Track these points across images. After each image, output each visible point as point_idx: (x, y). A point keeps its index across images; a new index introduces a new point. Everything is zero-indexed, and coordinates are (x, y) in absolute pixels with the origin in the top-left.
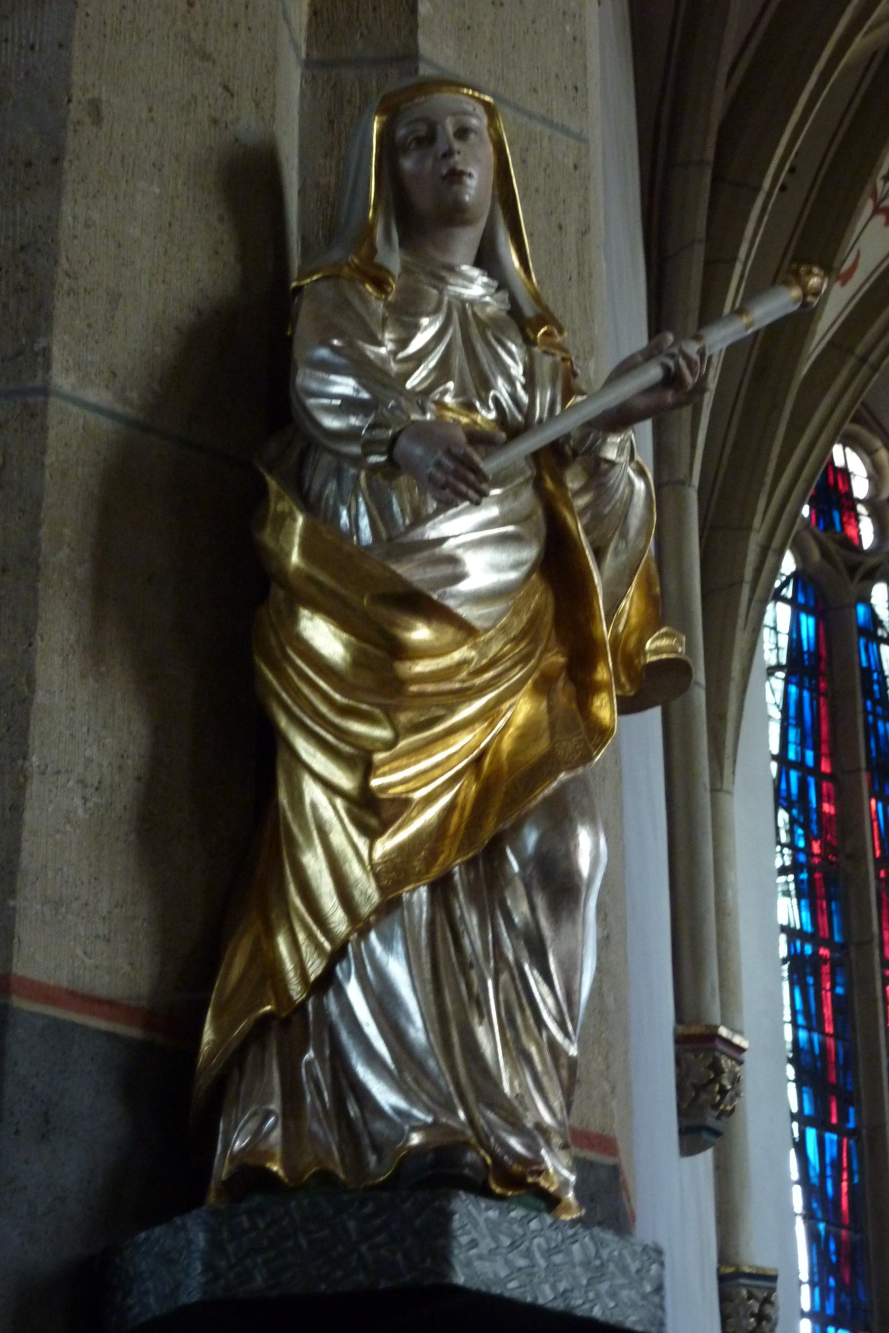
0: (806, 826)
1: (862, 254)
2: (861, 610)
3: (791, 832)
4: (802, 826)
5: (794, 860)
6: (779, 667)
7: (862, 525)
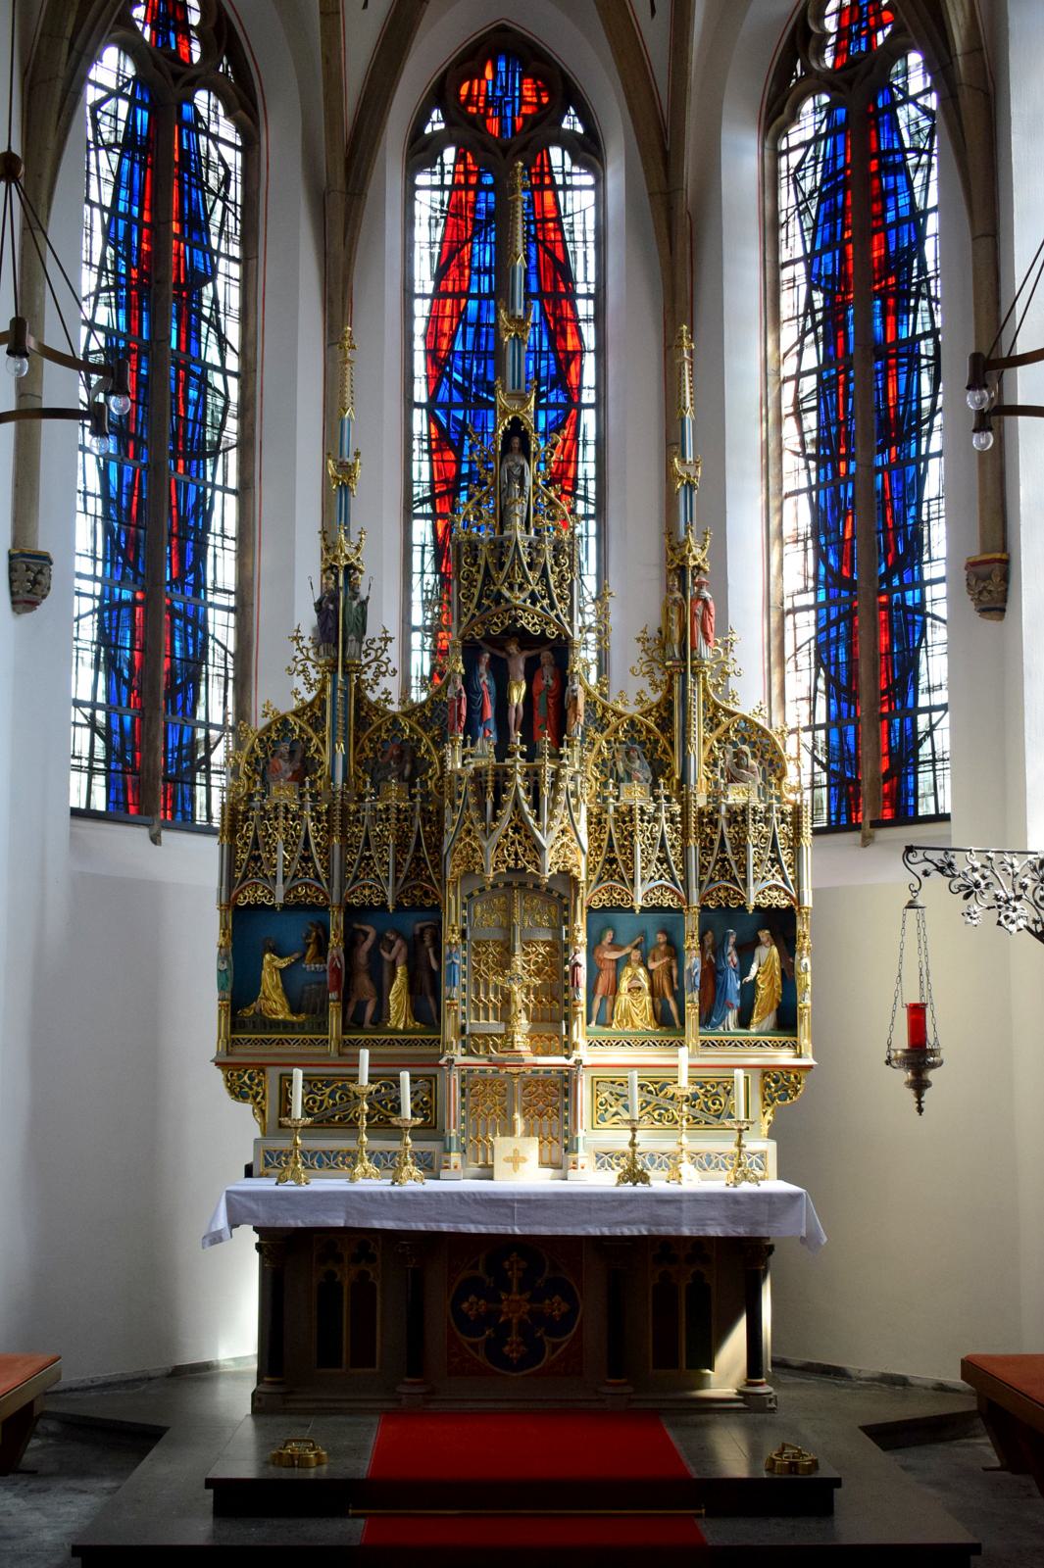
2: (187, 109)
3: (115, 263)
4: (124, 259)
6: (116, 144)
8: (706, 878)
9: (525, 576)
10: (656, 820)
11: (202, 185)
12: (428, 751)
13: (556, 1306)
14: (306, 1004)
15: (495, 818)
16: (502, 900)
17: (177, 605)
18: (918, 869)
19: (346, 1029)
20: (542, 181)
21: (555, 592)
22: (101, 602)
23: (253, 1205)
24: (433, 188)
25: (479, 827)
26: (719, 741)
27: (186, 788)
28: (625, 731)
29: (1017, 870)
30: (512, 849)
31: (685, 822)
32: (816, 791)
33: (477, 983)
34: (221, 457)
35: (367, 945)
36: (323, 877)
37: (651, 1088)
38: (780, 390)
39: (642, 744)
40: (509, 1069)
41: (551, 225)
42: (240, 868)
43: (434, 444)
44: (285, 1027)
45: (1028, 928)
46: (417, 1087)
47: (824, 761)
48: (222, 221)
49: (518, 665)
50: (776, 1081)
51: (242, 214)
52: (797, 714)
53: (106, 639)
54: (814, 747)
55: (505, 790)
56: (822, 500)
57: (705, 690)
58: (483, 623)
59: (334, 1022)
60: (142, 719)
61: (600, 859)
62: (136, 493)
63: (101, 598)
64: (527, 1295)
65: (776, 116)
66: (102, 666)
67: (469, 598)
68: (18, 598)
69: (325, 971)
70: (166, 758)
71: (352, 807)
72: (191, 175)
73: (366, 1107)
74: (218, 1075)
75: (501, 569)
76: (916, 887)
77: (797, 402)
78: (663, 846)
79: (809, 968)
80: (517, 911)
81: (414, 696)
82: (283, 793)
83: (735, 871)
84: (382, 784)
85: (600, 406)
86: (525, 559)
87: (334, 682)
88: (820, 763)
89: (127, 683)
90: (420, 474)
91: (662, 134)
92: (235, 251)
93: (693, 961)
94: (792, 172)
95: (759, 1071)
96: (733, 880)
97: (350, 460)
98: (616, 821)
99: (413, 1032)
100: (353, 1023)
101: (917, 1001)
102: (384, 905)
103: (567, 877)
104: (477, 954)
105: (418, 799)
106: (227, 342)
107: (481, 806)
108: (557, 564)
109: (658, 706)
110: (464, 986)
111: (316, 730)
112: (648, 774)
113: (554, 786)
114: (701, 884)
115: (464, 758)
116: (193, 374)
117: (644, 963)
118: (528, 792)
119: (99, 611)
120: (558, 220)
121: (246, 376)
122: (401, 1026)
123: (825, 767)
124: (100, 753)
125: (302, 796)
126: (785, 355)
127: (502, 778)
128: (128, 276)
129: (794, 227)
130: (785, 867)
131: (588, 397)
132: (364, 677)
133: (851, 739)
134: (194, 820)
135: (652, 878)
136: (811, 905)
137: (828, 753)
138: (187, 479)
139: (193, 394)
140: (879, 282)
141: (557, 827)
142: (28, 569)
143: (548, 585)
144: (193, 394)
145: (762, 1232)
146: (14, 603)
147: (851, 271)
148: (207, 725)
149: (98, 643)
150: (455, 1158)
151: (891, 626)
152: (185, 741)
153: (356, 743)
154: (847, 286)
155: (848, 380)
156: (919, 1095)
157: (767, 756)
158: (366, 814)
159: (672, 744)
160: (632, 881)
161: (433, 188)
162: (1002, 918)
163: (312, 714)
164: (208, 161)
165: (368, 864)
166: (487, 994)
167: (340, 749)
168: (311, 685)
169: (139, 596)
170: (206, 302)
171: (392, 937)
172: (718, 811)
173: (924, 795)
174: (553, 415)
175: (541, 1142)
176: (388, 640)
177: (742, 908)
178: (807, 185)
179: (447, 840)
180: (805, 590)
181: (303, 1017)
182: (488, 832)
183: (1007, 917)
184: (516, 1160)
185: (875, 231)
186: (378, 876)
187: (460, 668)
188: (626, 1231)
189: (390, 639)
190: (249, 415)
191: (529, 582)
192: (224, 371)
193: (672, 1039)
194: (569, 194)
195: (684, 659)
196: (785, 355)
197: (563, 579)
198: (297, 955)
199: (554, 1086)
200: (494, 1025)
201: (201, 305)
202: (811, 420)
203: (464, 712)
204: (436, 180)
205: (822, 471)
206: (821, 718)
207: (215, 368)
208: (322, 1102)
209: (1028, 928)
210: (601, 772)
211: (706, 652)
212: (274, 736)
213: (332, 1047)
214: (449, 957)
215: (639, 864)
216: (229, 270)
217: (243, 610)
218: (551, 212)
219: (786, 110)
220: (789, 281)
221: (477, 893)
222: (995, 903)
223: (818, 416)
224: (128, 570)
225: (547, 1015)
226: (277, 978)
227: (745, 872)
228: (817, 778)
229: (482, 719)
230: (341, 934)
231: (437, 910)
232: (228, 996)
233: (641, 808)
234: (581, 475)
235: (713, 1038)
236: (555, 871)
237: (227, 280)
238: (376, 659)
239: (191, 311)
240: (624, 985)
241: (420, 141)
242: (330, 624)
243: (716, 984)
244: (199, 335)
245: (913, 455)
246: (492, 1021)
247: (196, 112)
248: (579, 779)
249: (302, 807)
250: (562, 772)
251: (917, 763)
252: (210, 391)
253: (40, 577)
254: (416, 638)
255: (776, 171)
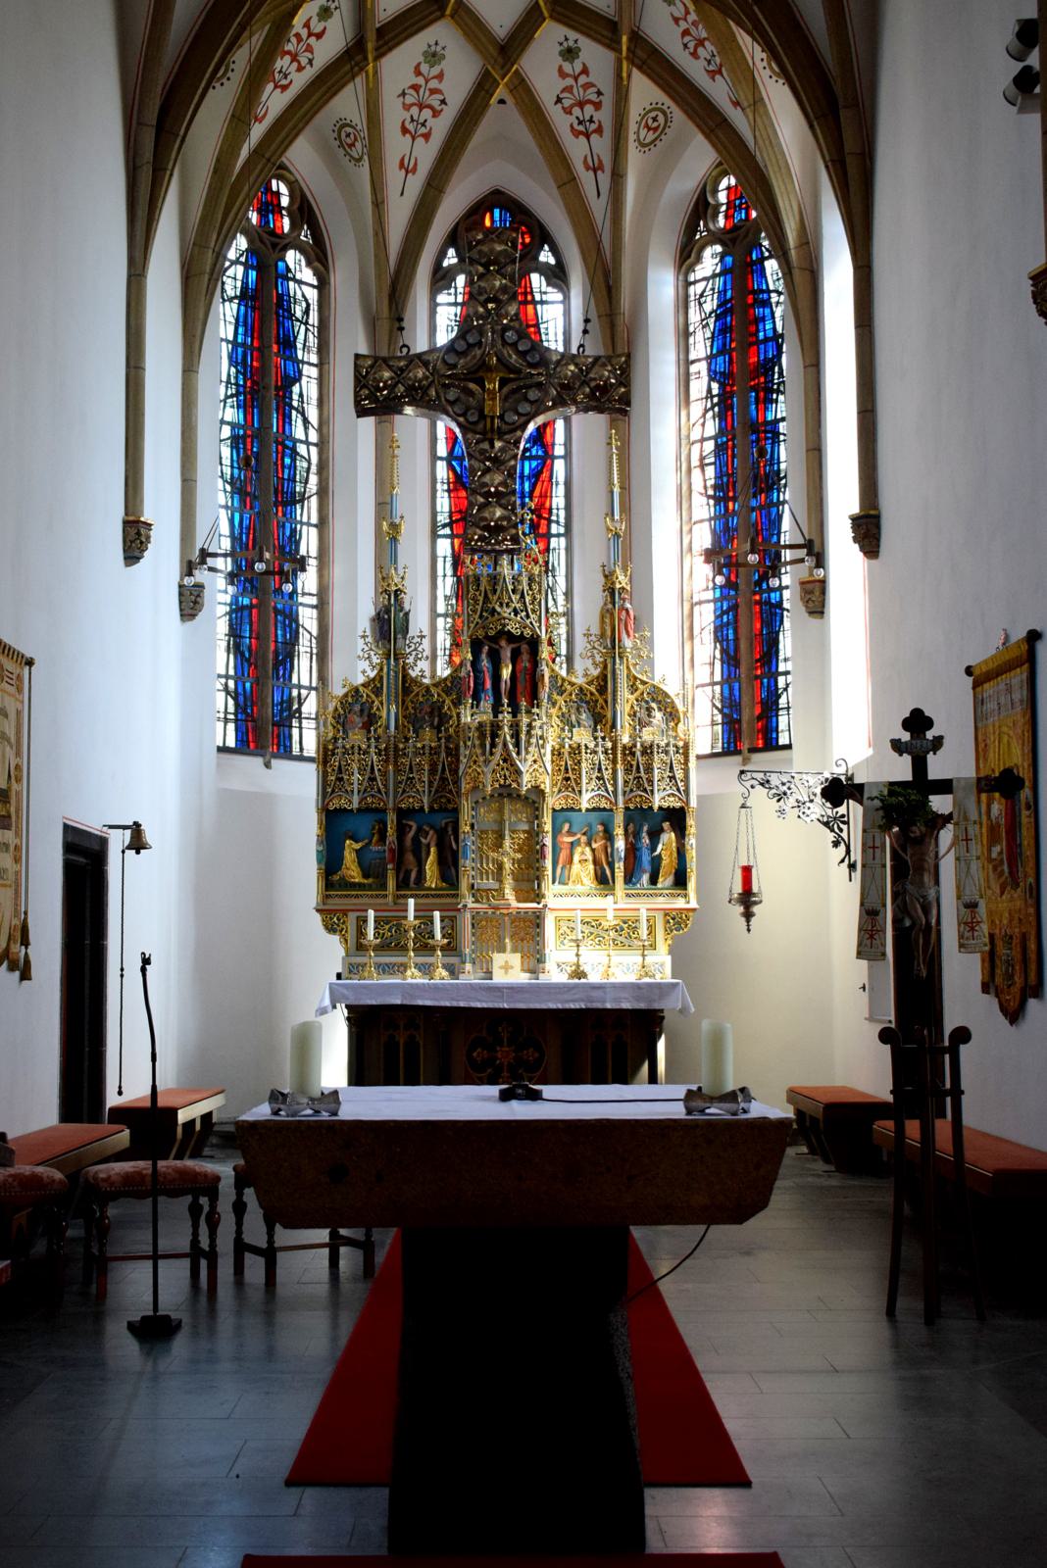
0: (244, 375)
1: (269, 111)
2: (281, 264)
3: (236, 378)
4: (241, 374)
5: (237, 391)
6: (236, 297)
7: (284, 221)
8: (628, 789)
9: (510, 598)
10: (595, 752)
11: (291, 316)
12: (449, 708)
13: (531, 1054)
14: (373, 872)
15: (492, 754)
16: (497, 804)
17: (279, 606)
18: (748, 784)
19: (399, 887)
20: (526, 297)
21: (530, 607)
22: (231, 608)
23: (345, 992)
24: (450, 304)
25: (482, 759)
26: (637, 700)
27: (286, 729)
28: (577, 694)
29: (811, 784)
30: (502, 773)
31: (614, 753)
32: (715, 727)
33: (481, 856)
34: (306, 502)
35: (411, 834)
36: (383, 790)
37: (593, 924)
38: (690, 449)
39: (587, 703)
40: (502, 911)
41: (532, 329)
42: (331, 783)
43: (451, 485)
44: (360, 886)
45: (818, 820)
46: (444, 924)
47: (720, 707)
48: (306, 340)
49: (506, 653)
50: (673, 919)
51: (319, 332)
52: (702, 674)
53: (234, 632)
54: (713, 697)
55: (498, 736)
56: (718, 527)
57: (628, 667)
58: (484, 628)
59: (391, 884)
60: (257, 684)
61: (560, 778)
62: (251, 532)
63: (231, 605)
64: (513, 1048)
65: (687, 256)
66: (232, 650)
67: (475, 611)
68: (185, 612)
69: (384, 851)
70: (273, 709)
71: (401, 746)
72: (284, 310)
73: (413, 935)
74: (318, 917)
75: (495, 593)
76: (747, 795)
77: (702, 458)
78: (600, 770)
79: (694, 846)
80: (506, 811)
81: (439, 673)
82: (357, 737)
83: (646, 785)
84: (420, 731)
85: (567, 456)
86: (510, 587)
87: (389, 664)
88: (717, 708)
89: (248, 660)
90: (442, 507)
91: (606, 275)
92: (314, 359)
93: (620, 844)
94: (697, 297)
95: (662, 912)
96: (645, 790)
97: (397, 521)
98: (570, 753)
99: (441, 889)
100: (403, 884)
101: (746, 864)
102: (422, 808)
103: (538, 791)
104: (481, 839)
105: (443, 740)
106: (309, 423)
107: (483, 746)
108: (531, 589)
109: (598, 678)
110: (473, 859)
111: (377, 696)
112: (592, 723)
113: (528, 733)
114: (625, 793)
115: (472, 715)
116: (288, 448)
117: (589, 844)
118: (512, 737)
119: (229, 613)
120: (537, 326)
121: (322, 445)
122: (433, 886)
123: (721, 711)
124: (231, 708)
125: (369, 739)
126: (693, 425)
127: (496, 728)
128: (244, 386)
129: (699, 336)
130: (679, 782)
131: (559, 450)
132: (407, 661)
133: (737, 693)
134: (291, 751)
135: (593, 790)
136: (695, 806)
137: (722, 701)
138: (284, 519)
139: (287, 461)
140: (754, 380)
141: (530, 758)
142: (191, 594)
143: (525, 603)
144: (287, 461)
145: (656, 1006)
146: (181, 615)
147: (735, 371)
148: (299, 687)
149: (229, 635)
150: (468, 966)
151: (762, 615)
152: (285, 698)
153: (403, 704)
154: (734, 381)
155: (734, 446)
156: (748, 921)
157: (668, 710)
158: (411, 750)
159: (606, 702)
160: (580, 792)
161: (450, 304)
162: (801, 814)
163: (374, 685)
164: (295, 299)
165: (411, 782)
166: (487, 865)
167: (393, 709)
168: (374, 667)
169: (254, 601)
170: (295, 397)
171: (427, 829)
172: (635, 746)
173: (782, 731)
174: (534, 464)
175: (522, 957)
176: (422, 637)
177: (651, 808)
178: (708, 307)
179: (462, 767)
180: (707, 589)
181: (370, 880)
182: (487, 762)
183: (804, 813)
184: (507, 968)
185: (751, 344)
186: (418, 790)
187: (469, 656)
188: (572, 1006)
189: (424, 637)
190: (325, 474)
191: (512, 601)
192: (307, 443)
193: (606, 893)
194: (545, 306)
195: (614, 648)
196: (693, 425)
197: (535, 598)
198: (366, 841)
199: (531, 921)
200: (492, 883)
201: (291, 399)
202: (710, 471)
203: (472, 685)
204: (452, 299)
205: (718, 507)
206: (718, 677)
207: (301, 442)
208: (384, 934)
209: (818, 820)
210: (561, 721)
211: (628, 643)
212: (350, 700)
213: (390, 898)
214: (464, 841)
215: (584, 780)
216: (310, 372)
217: (322, 607)
218: (532, 320)
219: (693, 255)
220: (696, 373)
221: (481, 800)
222: (796, 804)
223: (716, 468)
224: (247, 585)
225: (526, 877)
226: (354, 855)
227: (652, 785)
228: (715, 719)
229: (483, 689)
230: (395, 828)
231: (456, 811)
232: (323, 867)
233: (586, 745)
234: (554, 506)
235: (633, 892)
236: (529, 786)
237: (309, 379)
238: (415, 649)
239: (285, 404)
240: (576, 858)
241: (441, 273)
242: (386, 628)
243: (635, 857)
244: (291, 420)
245: (775, 501)
246: (491, 881)
247: (287, 267)
248: (545, 727)
249: (369, 747)
250: (534, 724)
251: (778, 709)
252: (298, 458)
253: (198, 599)
254: (440, 622)
255: (687, 296)
